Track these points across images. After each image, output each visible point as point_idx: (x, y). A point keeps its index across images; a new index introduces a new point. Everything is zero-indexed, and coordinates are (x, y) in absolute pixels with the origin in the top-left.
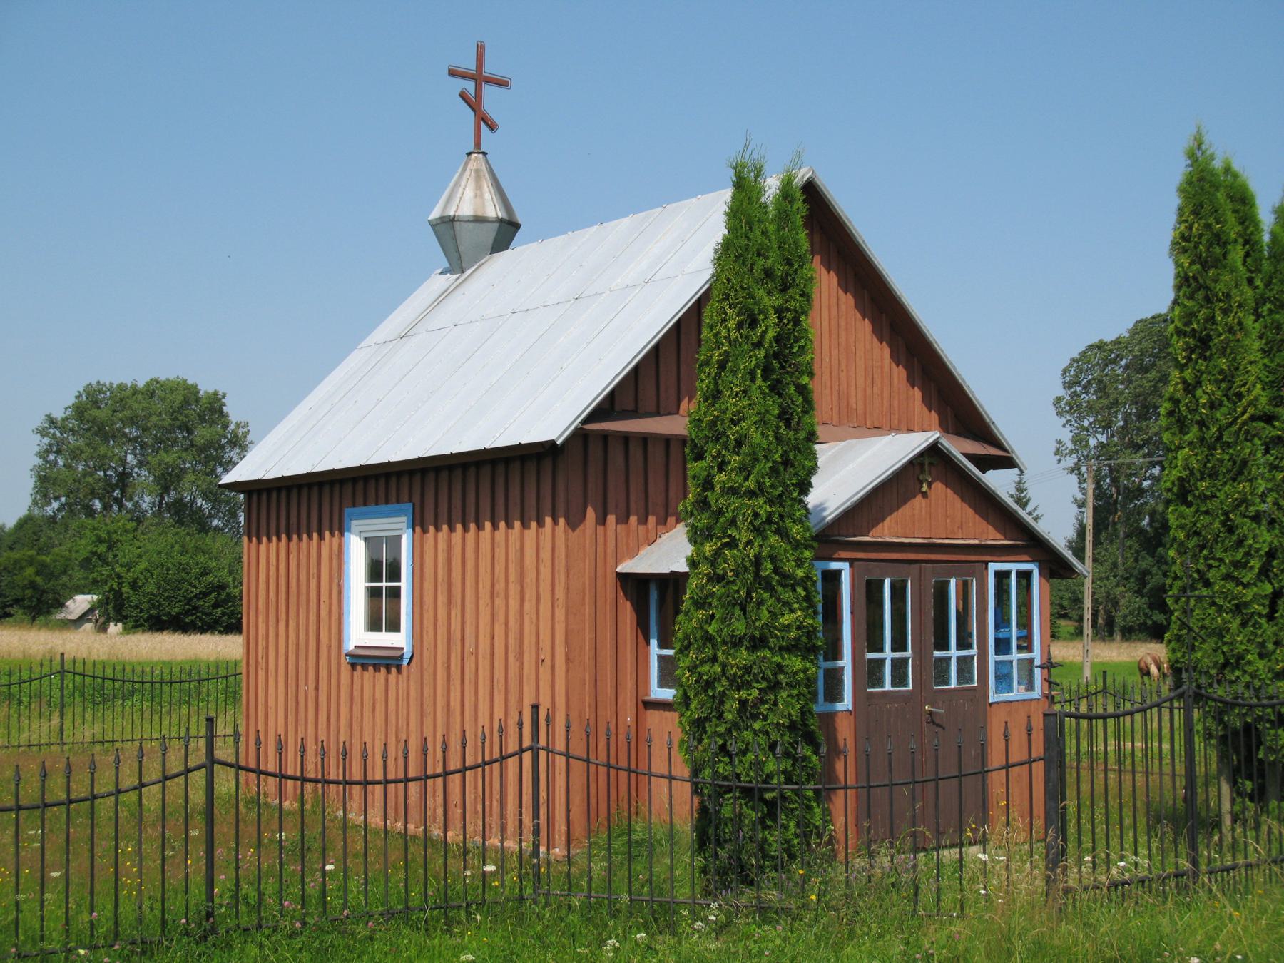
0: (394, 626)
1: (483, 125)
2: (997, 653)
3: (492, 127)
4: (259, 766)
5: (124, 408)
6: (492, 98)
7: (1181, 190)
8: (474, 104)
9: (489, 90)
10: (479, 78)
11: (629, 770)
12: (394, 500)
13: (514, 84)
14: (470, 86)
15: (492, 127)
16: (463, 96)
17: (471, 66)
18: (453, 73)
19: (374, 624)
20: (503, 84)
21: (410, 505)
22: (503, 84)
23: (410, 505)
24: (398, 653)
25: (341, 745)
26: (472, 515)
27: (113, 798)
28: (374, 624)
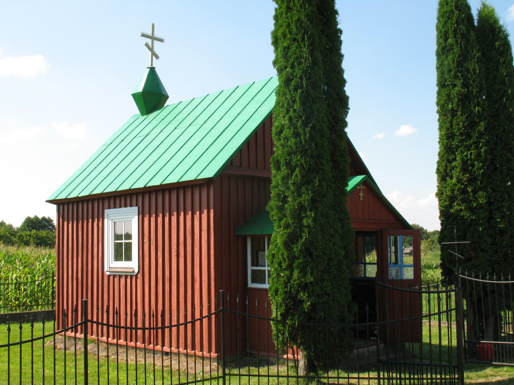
0: (129, 258)
1: (154, 57)
2: (253, 265)
3: (157, 57)
4: (98, 321)
5: (459, 124)
6: (158, 46)
7: (437, 93)
8: (151, 49)
9: (156, 42)
10: (153, 38)
11: (98, 323)
12: (119, 207)
13: (165, 40)
14: (149, 41)
15: (157, 57)
16: (147, 45)
17: (150, 33)
18: (143, 35)
19: (118, 257)
20: (162, 41)
21: (137, 208)
22: (162, 41)
23: (137, 208)
24: (131, 270)
25: (115, 309)
26: (190, 208)
27: (42, 340)
28: (118, 257)
